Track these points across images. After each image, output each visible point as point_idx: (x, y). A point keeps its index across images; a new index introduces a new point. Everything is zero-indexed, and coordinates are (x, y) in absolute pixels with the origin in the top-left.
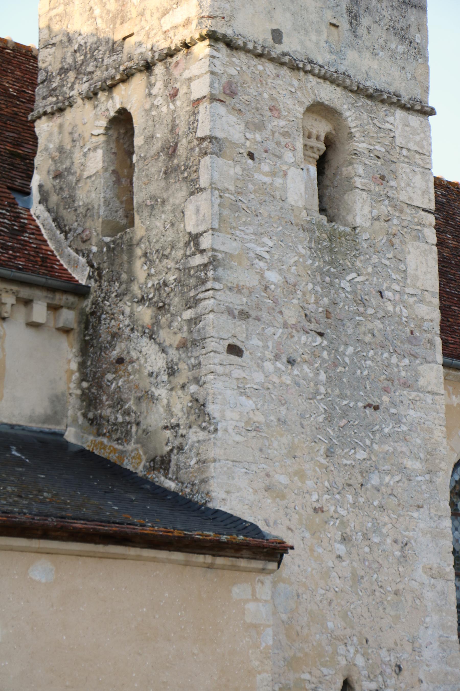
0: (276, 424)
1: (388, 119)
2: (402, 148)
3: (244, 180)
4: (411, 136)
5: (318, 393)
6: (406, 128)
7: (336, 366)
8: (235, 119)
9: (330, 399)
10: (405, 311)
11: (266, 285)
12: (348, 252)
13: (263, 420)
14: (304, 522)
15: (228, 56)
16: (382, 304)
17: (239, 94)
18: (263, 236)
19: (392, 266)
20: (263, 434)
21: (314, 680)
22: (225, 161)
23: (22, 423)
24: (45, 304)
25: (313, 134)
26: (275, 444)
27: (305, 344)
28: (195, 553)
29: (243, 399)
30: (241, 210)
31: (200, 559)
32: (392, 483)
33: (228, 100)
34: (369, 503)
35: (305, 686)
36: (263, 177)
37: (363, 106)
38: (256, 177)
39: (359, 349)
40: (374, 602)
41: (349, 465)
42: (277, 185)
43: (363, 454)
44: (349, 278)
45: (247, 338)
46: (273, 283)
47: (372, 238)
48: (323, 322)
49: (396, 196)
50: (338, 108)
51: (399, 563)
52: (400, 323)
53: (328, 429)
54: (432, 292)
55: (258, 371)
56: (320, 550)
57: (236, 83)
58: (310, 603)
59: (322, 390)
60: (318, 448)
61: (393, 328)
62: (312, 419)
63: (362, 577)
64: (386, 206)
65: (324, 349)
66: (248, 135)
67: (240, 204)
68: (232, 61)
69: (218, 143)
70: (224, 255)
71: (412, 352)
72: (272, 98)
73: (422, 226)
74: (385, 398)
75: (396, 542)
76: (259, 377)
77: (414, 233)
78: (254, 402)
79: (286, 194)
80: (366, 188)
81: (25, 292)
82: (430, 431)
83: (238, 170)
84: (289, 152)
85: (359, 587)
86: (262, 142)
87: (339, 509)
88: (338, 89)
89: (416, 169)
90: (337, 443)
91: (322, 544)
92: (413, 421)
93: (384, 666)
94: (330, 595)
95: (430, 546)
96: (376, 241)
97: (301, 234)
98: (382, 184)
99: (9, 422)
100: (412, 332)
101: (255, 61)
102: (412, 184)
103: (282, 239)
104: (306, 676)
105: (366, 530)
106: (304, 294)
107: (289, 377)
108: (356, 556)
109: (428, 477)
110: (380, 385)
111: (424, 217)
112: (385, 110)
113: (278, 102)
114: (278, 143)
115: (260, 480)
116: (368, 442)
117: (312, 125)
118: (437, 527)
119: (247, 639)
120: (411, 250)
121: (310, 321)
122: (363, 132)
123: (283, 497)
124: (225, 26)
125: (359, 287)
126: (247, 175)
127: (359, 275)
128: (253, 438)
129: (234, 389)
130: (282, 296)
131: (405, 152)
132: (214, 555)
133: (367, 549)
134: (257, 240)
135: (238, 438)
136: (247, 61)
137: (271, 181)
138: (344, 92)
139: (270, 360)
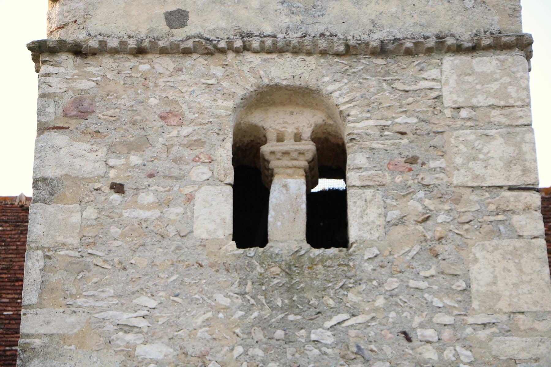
2: (459, 108)
8: (87, 146)
12: (330, 284)
16: (411, 352)
17: (97, 111)
19: (435, 287)
30: (92, 266)
36: (141, 212)
38: (126, 215)
47: (386, 253)
50: (312, 83)
54: (535, 312)
64: (420, 200)
66: (112, 162)
67: (89, 259)
73: (510, 213)
77: (486, 228)
80: (371, 183)
84: (201, 167)
86: (144, 165)
88: (308, 59)
89: (492, 132)
96: (396, 256)
97: (223, 277)
98: (410, 170)
101: (133, 61)
102: (481, 156)
103: (178, 291)
113: (178, 104)
122: (368, 105)
127: (354, 316)
131: (464, 113)
134: (122, 304)
136: (114, 65)
137: (159, 214)
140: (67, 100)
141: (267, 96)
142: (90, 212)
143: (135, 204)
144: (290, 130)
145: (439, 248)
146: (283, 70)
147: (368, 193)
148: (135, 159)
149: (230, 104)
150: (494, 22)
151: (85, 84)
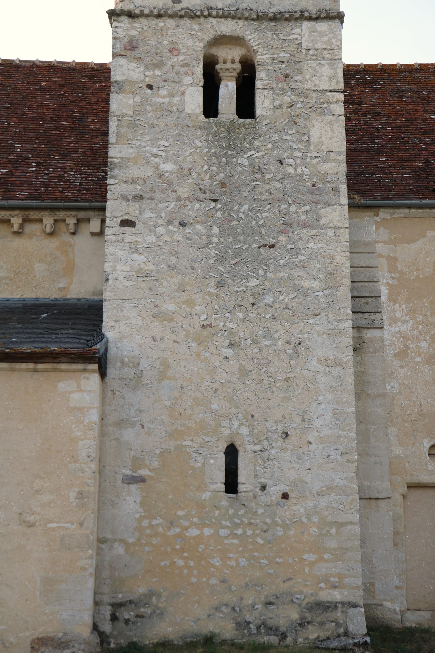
0: (167, 269)
1: (294, 32)
2: (309, 49)
3: (143, 105)
4: (318, 39)
5: (210, 242)
6: (313, 34)
7: (230, 221)
8: (135, 65)
9: (222, 245)
10: (306, 171)
11: (160, 174)
13: (154, 268)
14: (191, 336)
15: (129, 23)
18: (159, 140)
19: (295, 139)
20: (153, 278)
21: (195, 445)
22: (124, 95)
23: (86, 297)
24: (100, 220)
25: (228, 60)
26: (165, 284)
27: (198, 210)
28: (18, 362)
29: (135, 256)
31: (24, 366)
32: (286, 300)
33: (128, 53)
34: (260, 317)
35: (186, 450)
36: (161, 99)
37: (266, 28)
38: (154, 100)
39: (255, 205)
40: (261, 388)
41: (241, 291)
42: (175, 102)
43: (256, 282)
44: (246, 156)
45: (140, 213)
46: (167, 171)
47: (273, 122)
48: (218, 191)
49: (302, 86)
50: (241, 35)
51: (291, 358)
52: (302, 180)
53: (219, 268)
55: (151, 235)
56: (207, 355)
57: (137, 40)
58: (194, 392)
59: (215, 240)
60: (208, 282)
61: (292, 185)
62: (203, 262)
63: (250, 371)
64: (289, 96)
65: (217, 210)
66: (147, 74)
67: (138, 122)
68: (134, 26)
69: (118, 84)
70: (120, 160)
71: (312, 200)
72: (172, 42)
73: (330, 103)
74: (282, 238)
75: (288, 343)
76: (151, 238)
78: (146, 257)
79: (184, 107)
80: (267, 87)
81: (81, 215)
82: (332, 257)
83: (138, 99)
85: (246, 378)
87: (228, 324)
89: (324, 62)
90: (227, 276)
91: (209, 350)
92: (312, 251)
93: (270, 434)
94: (215, 386)
95: (326, 343)
97: (198, 132)
98: (285, 81)
99: (77, 297)
101: (156, 21)
102: (318, 75)
104: (189, 443)
105: (256, 336)
106: (199, 174)
107: (181, 235)
108: (244, 356)
109: (327, 292)
110: (277, 229)
111: (331, 96)
112: (291, 26)
113: (177, 44)
114: (177, 73)
115: (148, 310)
116: (261, 272)
117: (228, 53)
118: (335, 328)
119: (71, 418)
120: (315, 124)
121: (205, 192)
122: (267, 47)
123: (171, 320)
124: (129, 4)
125: (257, 160)
126: (146, 100)
128: (143, 282)
129: (126, 250)
130: (177, 179)
131: (311, 52)
132: (35, 363)
133: (256, 351)
134: (153, 144)
135: (129, 283)
137: (169, 101)
138: (246, 23)
139: (163, 225)
140: (125, 41)
141: (220, 40)
142: (138, 99)
143: (158, 95)
144: (229, 57)
146: (227, 27)
147: (266, 92)
149: (202, 45)
151: (134, 33)
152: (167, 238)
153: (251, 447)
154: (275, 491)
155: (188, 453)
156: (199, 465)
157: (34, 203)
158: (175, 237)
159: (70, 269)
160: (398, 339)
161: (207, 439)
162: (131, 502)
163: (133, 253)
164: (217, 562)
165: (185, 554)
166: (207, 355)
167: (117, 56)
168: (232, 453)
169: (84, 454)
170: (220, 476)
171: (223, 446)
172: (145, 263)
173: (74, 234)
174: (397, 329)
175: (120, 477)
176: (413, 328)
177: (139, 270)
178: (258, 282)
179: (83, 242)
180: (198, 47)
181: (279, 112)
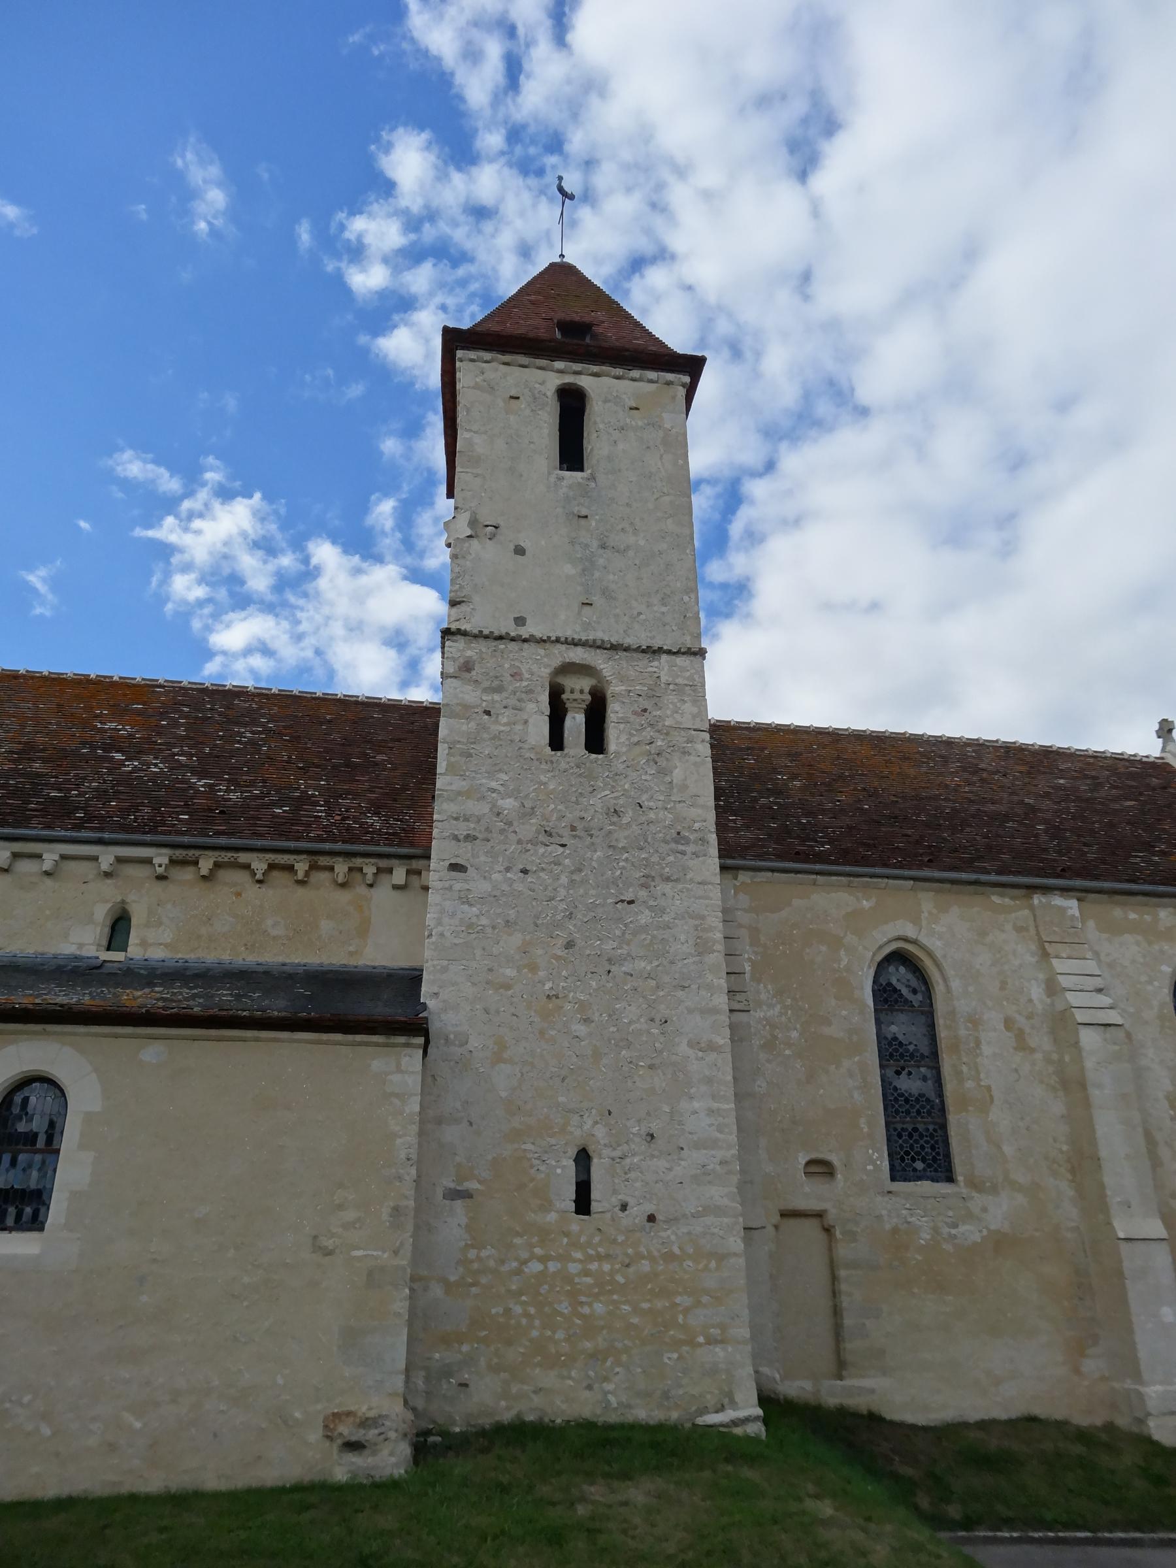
50: (593, 664)
76: (486, 886)
81: (383, 863)
83: (472, 725)
100: (679, 833)
104: (529, 1146)
131: (671, 687)
140: (462, 660)
141: (568, 669)
142: (472, 725)
143: (497, 722)
144: (578, 687)
145: (657, 759)
146: (577, 655)
147: (622, 726)
148: (497, 697)
149: (548, 671)
150: (688, 642)
151: (469, 653)
152: (505, 887)
153: (606, 1152)
154: (638, 1211)
155: (529, 1160)
156: (543, 1176)
157: (327, 846)
158: (515, 886)
159: (363, 930)
160: (764, 1026)
161: (553, 1141)
162: (454, 1224)
163: (463, 903)
164: (564, 1307)
165: (524, 1298)
166: (553, 1033)
167: (447, 677)
168: (583, 1158)
169: (403, 1156)
170: (570, 1192)
171: (572, 1152)
172: (477, 916)
173: (371, 886)
174: (762, 1015)
175: (439, 1192)
176: (781, 1014)
177: (470, 926)
178: (615, 945)
179: (383, 898)
180: (546, 672)
181: (637, 750)
